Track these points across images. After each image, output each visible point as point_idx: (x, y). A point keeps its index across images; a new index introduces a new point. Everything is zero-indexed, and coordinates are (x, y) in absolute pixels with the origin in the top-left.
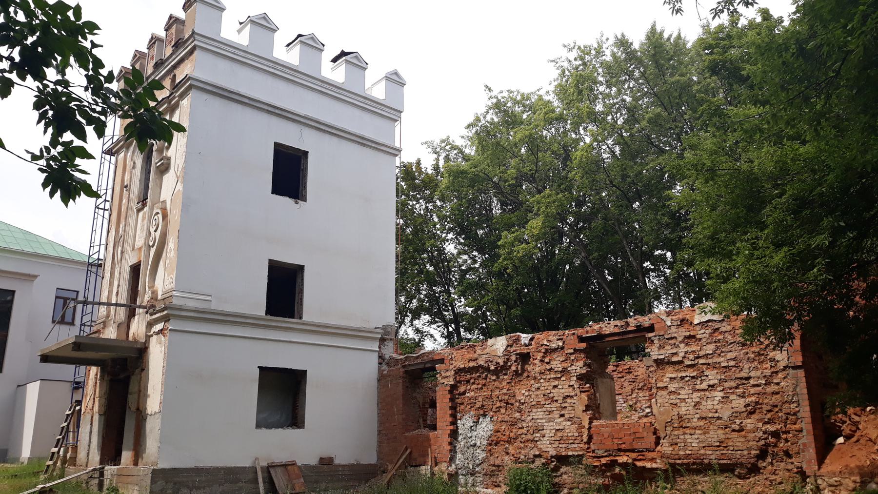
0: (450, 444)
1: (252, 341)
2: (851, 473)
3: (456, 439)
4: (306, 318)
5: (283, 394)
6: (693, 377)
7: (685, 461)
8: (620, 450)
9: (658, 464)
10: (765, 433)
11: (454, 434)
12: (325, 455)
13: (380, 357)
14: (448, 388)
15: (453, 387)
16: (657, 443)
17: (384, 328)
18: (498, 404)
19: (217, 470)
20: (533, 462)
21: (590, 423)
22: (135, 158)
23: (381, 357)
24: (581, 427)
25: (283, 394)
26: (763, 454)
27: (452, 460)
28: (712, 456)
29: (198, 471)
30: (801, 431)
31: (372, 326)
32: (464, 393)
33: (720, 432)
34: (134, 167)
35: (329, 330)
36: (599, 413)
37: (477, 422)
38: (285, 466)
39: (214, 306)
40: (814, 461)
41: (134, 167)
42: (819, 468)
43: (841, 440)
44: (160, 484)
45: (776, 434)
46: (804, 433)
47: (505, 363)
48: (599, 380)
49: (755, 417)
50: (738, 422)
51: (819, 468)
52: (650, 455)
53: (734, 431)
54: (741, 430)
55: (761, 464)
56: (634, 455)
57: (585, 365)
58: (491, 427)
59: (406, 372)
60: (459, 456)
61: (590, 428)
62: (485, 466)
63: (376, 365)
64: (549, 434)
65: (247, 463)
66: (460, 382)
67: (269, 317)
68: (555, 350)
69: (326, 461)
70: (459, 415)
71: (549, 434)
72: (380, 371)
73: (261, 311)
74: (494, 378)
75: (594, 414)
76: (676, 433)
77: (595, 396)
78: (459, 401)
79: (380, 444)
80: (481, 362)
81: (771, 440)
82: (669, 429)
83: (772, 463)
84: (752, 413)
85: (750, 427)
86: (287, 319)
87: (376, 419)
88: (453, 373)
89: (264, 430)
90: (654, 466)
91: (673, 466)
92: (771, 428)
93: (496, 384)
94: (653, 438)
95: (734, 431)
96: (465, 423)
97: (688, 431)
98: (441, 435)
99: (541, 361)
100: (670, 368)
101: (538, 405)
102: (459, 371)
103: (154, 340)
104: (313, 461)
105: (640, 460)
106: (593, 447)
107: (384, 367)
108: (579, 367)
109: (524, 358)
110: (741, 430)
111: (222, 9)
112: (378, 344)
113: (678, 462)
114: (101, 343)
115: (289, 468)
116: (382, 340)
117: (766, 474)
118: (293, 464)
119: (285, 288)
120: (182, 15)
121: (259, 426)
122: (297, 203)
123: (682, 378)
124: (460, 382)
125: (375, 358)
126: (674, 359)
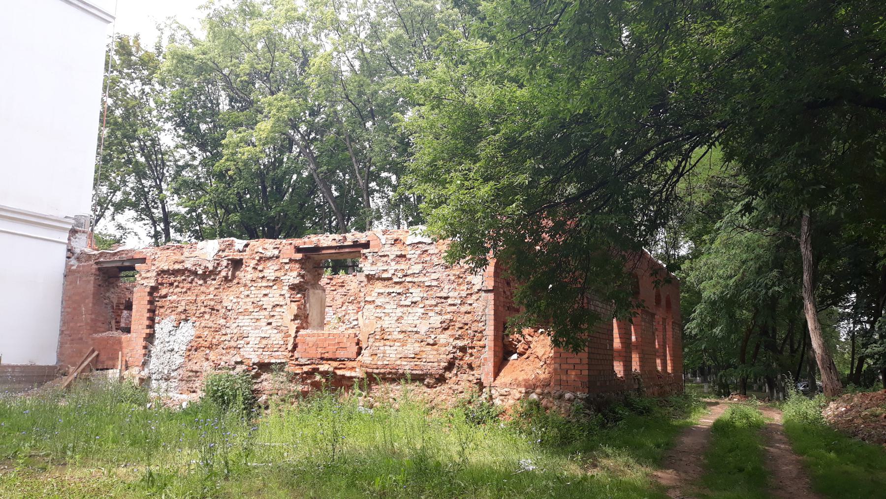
1: (10, 236)
2: (519, 385)
3: (152, 343)
6: (399, 294)
7: (382, 371)
8: (322, 359)
9: (358, 373)
10: (454, 347)
11: (150, 338)
13: (69, 250)
17: (76, 218)
18: (203, 309)
20: (234, 368)
21: (297, 332)
26: (450, 366)
27: (145, 364)
28: (407, 367)
31: (61, 215)
32: (165, 296)
33: (417, 345)
36: (307, 322)
42: (495, 380)
43: (515, 356)
45: (463, 349)
46: (487, 349)
48: (311, 291)
49: (448, 332)
50: (433, 336)
52: (350, 364)
55: (448, 375)
56: (335, 364)
57: (299, 275)
58: (193, 332)
59: (99, 269)
60: (153, 360)
61: (296, 337)
63: (63, 259)
66: (162, 284)
70: (157, 319)
72: (67, 265)
75: (302, 324)
76: (377, 344)
77: (305, 306)
79: (61, 345)
80: (188, 265)
82: (371, 340)
83: (456, 375)
84: (445, 329)
88: (155, 274)
90: (353, 374)
92: (460, 343)
95: (428, 344)
96: (163, 328)
97: (388, 343)
98: (134, 341)
106: (296, 355)
107: (73, 261)
109: (237, 264)
112: (67, 235)
123: (389, 294)
124: (162, 284)
125: (62, 251)
126: (385, 275)
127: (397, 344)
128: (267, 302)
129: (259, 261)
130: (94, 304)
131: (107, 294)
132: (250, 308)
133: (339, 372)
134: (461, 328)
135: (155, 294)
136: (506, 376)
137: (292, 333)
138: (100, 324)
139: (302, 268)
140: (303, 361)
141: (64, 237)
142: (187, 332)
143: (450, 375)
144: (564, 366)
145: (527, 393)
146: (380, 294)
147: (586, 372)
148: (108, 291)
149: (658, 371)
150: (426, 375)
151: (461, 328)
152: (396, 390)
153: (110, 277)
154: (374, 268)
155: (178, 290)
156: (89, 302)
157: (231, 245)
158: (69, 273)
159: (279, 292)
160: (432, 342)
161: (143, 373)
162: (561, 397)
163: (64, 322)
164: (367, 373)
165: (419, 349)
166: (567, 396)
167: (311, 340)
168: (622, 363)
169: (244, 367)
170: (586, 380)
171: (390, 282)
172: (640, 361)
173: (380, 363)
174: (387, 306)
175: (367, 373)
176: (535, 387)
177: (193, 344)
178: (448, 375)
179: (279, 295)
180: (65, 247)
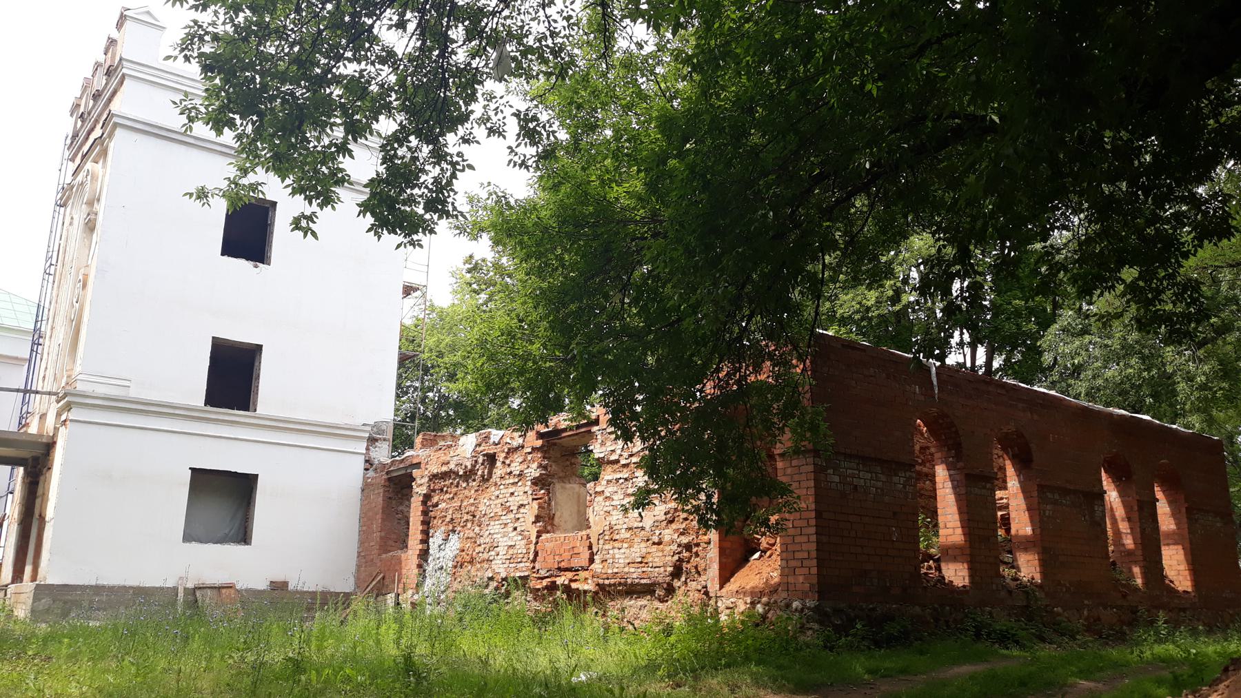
0: (420, 566)
2: (745, 594)
5: (225, 500)
7: (612, 581)
8: (559, 569)
9: (589, 586)
10: (679, 546)
11: (424, 555)
12: (279, 578)
13: (367, 461)
14: (421, 498)
15: (427, 497)
17: (376, 425)
18: (466, 517)
19: (125, 589)
20: (487, 586)
21: (538, 537)
23: (368, 461)
25: (225, 500)
26: (677, 572)
27: (419, 586)
28: (634, 575)
29: (98, 589)
30: (709, 543)
31: (358, 422)
32: (436, 505)
33: (643, 545)
36: (552, 525)
37: (446, 540)
38: (218, 588)
39: (133, 393)
40: (717, 580)
43: (757, 555)
44: (45, 602)
45: (688, 547)
46: (712, 545)
48: (558, 486)
49: (674, 526)
50: (657, 532)
52: (582, 574)
53: (654, 543)
54: (659, 543)
55: (676, 583)
56: (570, 575)
57: (540, 466)
58: (458, 545)
60: (428, 582)
61: (537, 543)
63: (362, 471)
64: (502, 550)
65: (170, 584)
66: (434, 491)
67: (209, 408)
68: (516, 449)
69: (279, 587)
70: (431, 531)
71: (502, 550)
73: (200, 400)
75: (545, 527)
76: (607, 547)
77: (549, 505)
79: (359, 566)
80: (452, 466)
81: (686, 554)
82: (601, 542)
83: (686, 583)
84: (671, 522)
85: (667, 538)
87: (357, 537)
89: (194, 545)
90: (586, 587)
91: (601, 587)
92: (685, 540)
93: (466, 492)
94: (586, 554)
95: (654, 543)
96: (435, 542)
97: (617, 545)
100: (609, 468)
102: (434, 477)
104: (262, 585)
105: (576, 581)
106: (537, 566)
107: (371, 473)
108: (534, 471)
109: (491, 459)
110: (659, 543)
112: (365, 445)
113: (607, 582)
114: (29, 439)
115: (224, 591)
116: (372, 440)
117: (680, 592)
119: (233, 375)
120: (115, 34)
121: (187, 538)
123: (617, 480)
124: (434, 491)
125: (360, 463)
126: (613, 458)
127: (625, 545)
128: (513, 502)
132: (499, 510)
133: (574, 585)
136: (733, 585)
137: (534, 539)
138: (391, 543)
140: (543, 573)
141: (361, 447)
144: (793, 563)
146: (609, 482)
147: (814, 571)
149: (1136, 589)
150: (653, 584)
151: (686, 519)
153: (402, 488)
154: (604, 449)
155: (448, 496)
156: (379, 516)
158: (366, 487)
160: (656, 539)
161: (416, 597)
162: (788, 606)
163: (362, 542)
164: (598, 585)
166: (796, 604)
168: (966, 565)
169: (495, 584)
172: (1041, 565)
175: (598, 585)
176: (762, 593)
177: (459, 559)
178: (676, 583)
179: (523, 494)
180: (362, 458)
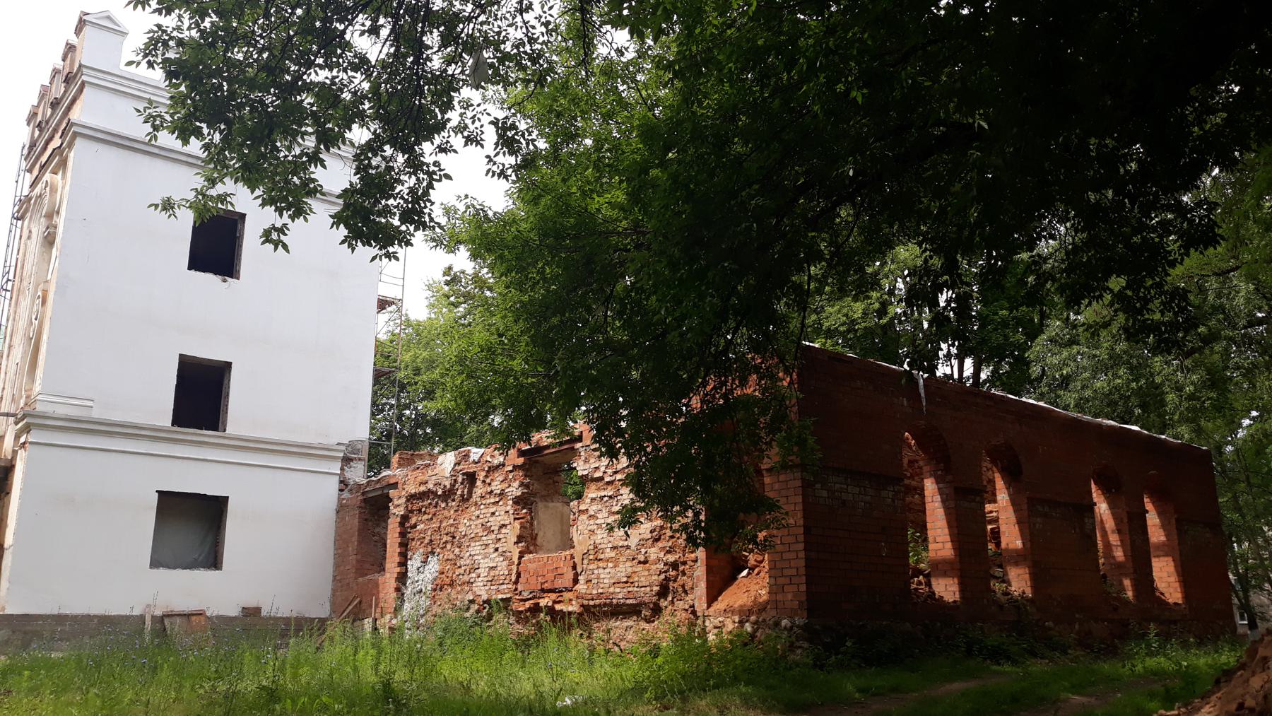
1: (148, 458)
2: (733, 612)
3: (405, 584)
4: (231, 428)
5: (193, 525)
6: (610, 497)
7: (597, 602)
8: (543, 590)
9: (574, 608)
10: (666, 564)
11: (402, 578)
12: (252, 604)
13: (341, 482)
14: (398, 520)
15: (405, 518)
16: (576, 581)
17: (351, 444)
18: (445, 538)
20: (468, 609)
21: (520, 558)
22: (32, 225)
23: (343, 483)
24: (512, 564)
25: (193, 525)
26: (664, 591)
27: (397, 610)
28: (619, 594)
29: (60, 619)
30: (696, 561)
31: (333, 441)
32: (415, 526)
33: (629, 564)
34: (29, 238)
35: (143, 432)
36: (535, 545)
37: (425, 562)
38: (188, 616)
39: (96, 414)
40: (704, 598)
41: (29, 238)
42: (709, 606)
43: (745, 573)
45: (675, 565)
46: (699, 563)
47: (453, 486)
48: (540, 505)
49: (660, 544)
50: (643, 551)
51: (709, 606)
52: (567, 595)
53: (640, 562)
54: (645, 562)
55: (663, 603)
56: (553, 596)
57: (522, 485)
58: (437, 567)
59: (365, 501)
60: (407, 605)
61: (519, 564)
62: (429, 617)
63: (337, 491)
65: (136, 612)
66: (412, 511)
67: (176, 428)
68: (497, 468)
69: (251, 613)
72: (340, 500)
73: (167, 421)
74: (443, 505)
75: (527, 547)
76: (591, 567)
77: (532, 524)
78: (410, 535)
79: (334, 591)
80: (430, 486)
81: (672, 573)
82: (586, 562)
83: (672, 602)
84: (657, 540)
85: (653, 557)
86: (204, 432)
88: (404, 500)
90: (570, 609)
92: (671, 558)
93: (445, 513)
95: (640, 562)
96: (413, 564)
97: (601, 564)
98: (388, 580)
99: (484, 481)
100: (593, 486)
101: (476, 538)
102: (411, 498)
103: (22, 454)
104: (233, 611)
105: (559, 602)
106: (520, 587)
107: (346, 494)
108: (515, 490)
109: (471, 478)
110: (645, 562)
111: (124, 34)
112: (339, 465)
113: (592, 603)
115: (194, 618)
116: (347, 460)
117: (666, 612)
118: (200, 614)
119: (201, 394)
120: (74, 40)
122: (225, 281)
123: (602, 498)
124: (412, 511)
125: (334, 483)
127: (610, 565)
128: (494, 523)
129: (488, 472)
130: (359, 543)
131: (377, 530)
133: (558, 607)
134: (672, 537)
135: (407, 525)
137: (516, 560)
139: (526, 476)
140: (526, 595)
141: (336, 468)
142: (434, 566)
143: (666, 603)
145: (741, 622)
146: (593, 499)
147: (803, 588)
148: (378, 525)
149: (1127, 602)
152: (618, 626)
154: (587, 466)
155: (426, 517)
156: (355, 539)
157: (467, 455)
158: (341, 509)
159: (503, 508)
160: (642, 558)
161: (394, 622)
162: (777, 624)
163: (337, 566)
164: (582, 606)
165: (630, 570)
166: (784, 622)
167: (531, 566)
168: (956, 580)
170: (804, 598)
171: (600, 484)
173: (595, 592)
174: (600, 516)
175: (582, 606)
176: (750, 612)
177: (439, 582)
178: (663, 603)
179: (503, 514)
180: (337, 479)
